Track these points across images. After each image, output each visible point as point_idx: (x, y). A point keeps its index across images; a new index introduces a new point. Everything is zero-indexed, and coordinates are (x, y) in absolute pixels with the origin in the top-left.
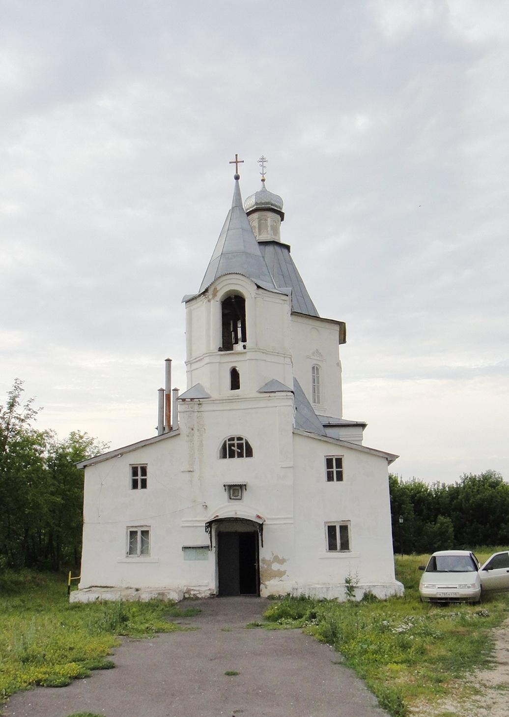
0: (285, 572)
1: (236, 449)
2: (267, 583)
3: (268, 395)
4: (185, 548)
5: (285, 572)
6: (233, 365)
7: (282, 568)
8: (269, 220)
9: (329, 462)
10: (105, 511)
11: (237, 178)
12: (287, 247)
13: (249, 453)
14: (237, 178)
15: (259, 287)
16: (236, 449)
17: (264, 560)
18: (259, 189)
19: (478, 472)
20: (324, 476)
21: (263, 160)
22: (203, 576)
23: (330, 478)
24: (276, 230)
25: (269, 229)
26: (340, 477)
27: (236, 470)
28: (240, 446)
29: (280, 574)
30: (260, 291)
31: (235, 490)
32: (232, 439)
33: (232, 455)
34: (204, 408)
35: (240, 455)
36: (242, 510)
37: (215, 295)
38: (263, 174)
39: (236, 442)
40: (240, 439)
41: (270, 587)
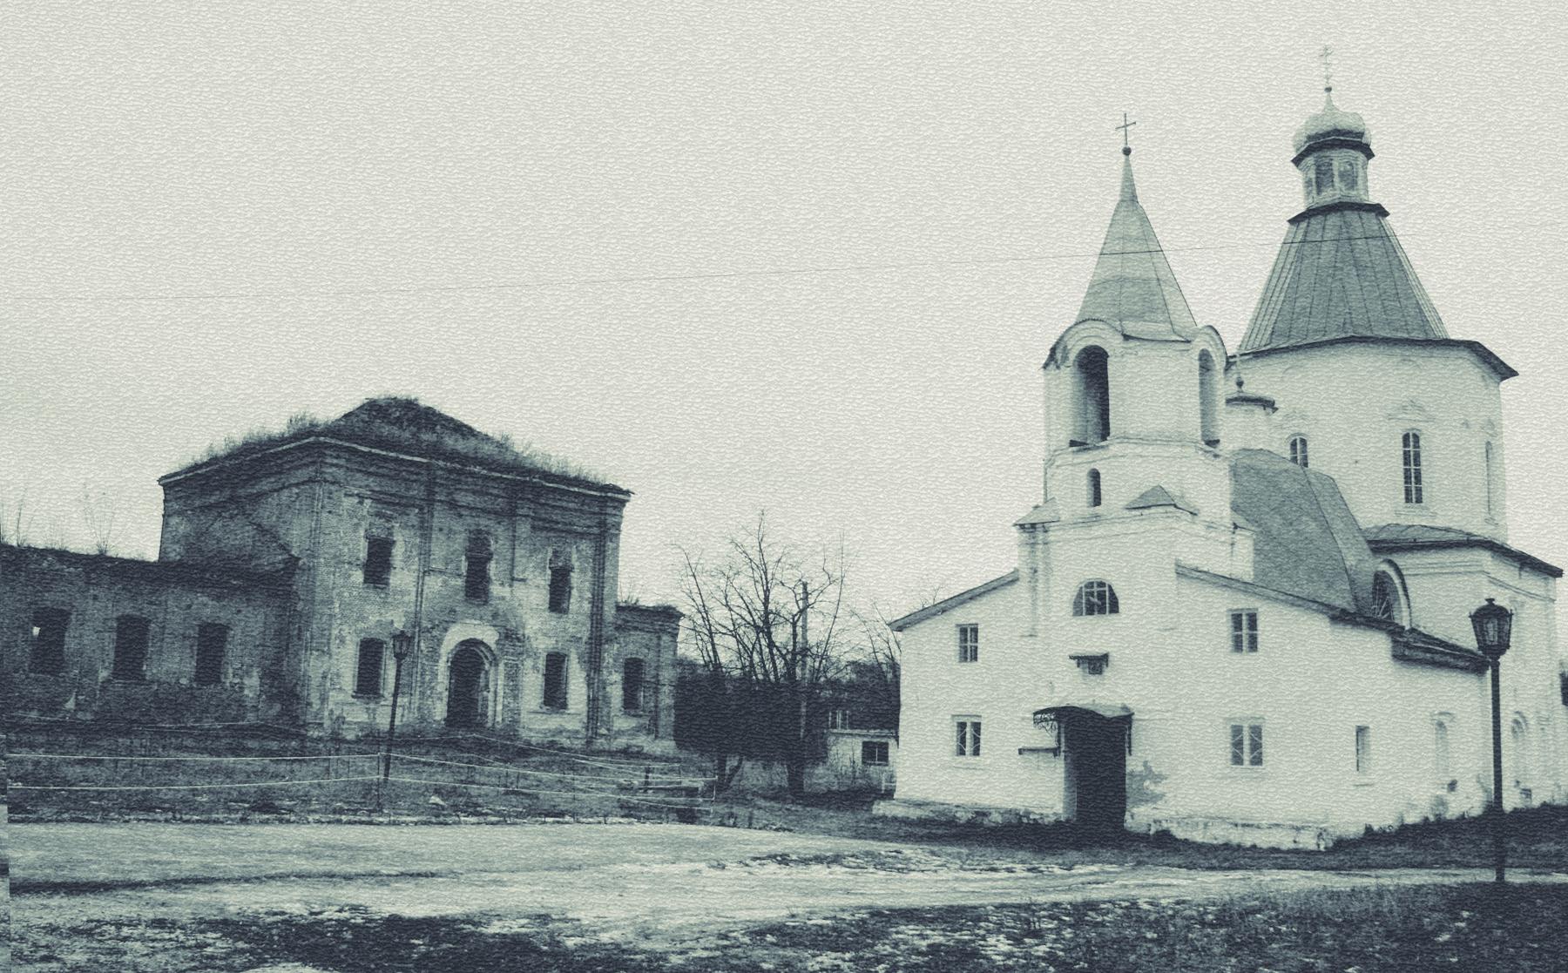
0: (1163, 795)
1: (1098, 600)
2: (1135, 810)
3: (1137, 512)
4: (1021, 751)
5: (1163, 795)
6: (1093, 466)
7: (1158, 789)
8: (1335, 163)
9: (1236, 619)
10: (931, 692)
11: (1127, 152)
12: (1380, 211)
13: (1114, 608)
14: (1127, 152)
15: (1127, 337)
16: (1098, 600)
17: (1131, 774)
18: (1319, 109)
19: (672, 604)
20: (1229, 644)
21: (1326, 52)
22: (1045, 792)
23: (1238, 646)
24: (1351, 179)
25: (1336, 179)
26: (1253, 646)
27: (1095, 634)
28: (1101, 596)
29: (1154, 798)
30: (1132, 344)
31: (1095, 664)
32: (1090, 585)
33: (1090, 612)
34: (1052, 536)
35: (1102, 611)
36: (1102, 696)
37: (1065, 358)
38: (1328, 78)
39: (1096, 589)
40: (1101, 584)
41: (1139, 817)
